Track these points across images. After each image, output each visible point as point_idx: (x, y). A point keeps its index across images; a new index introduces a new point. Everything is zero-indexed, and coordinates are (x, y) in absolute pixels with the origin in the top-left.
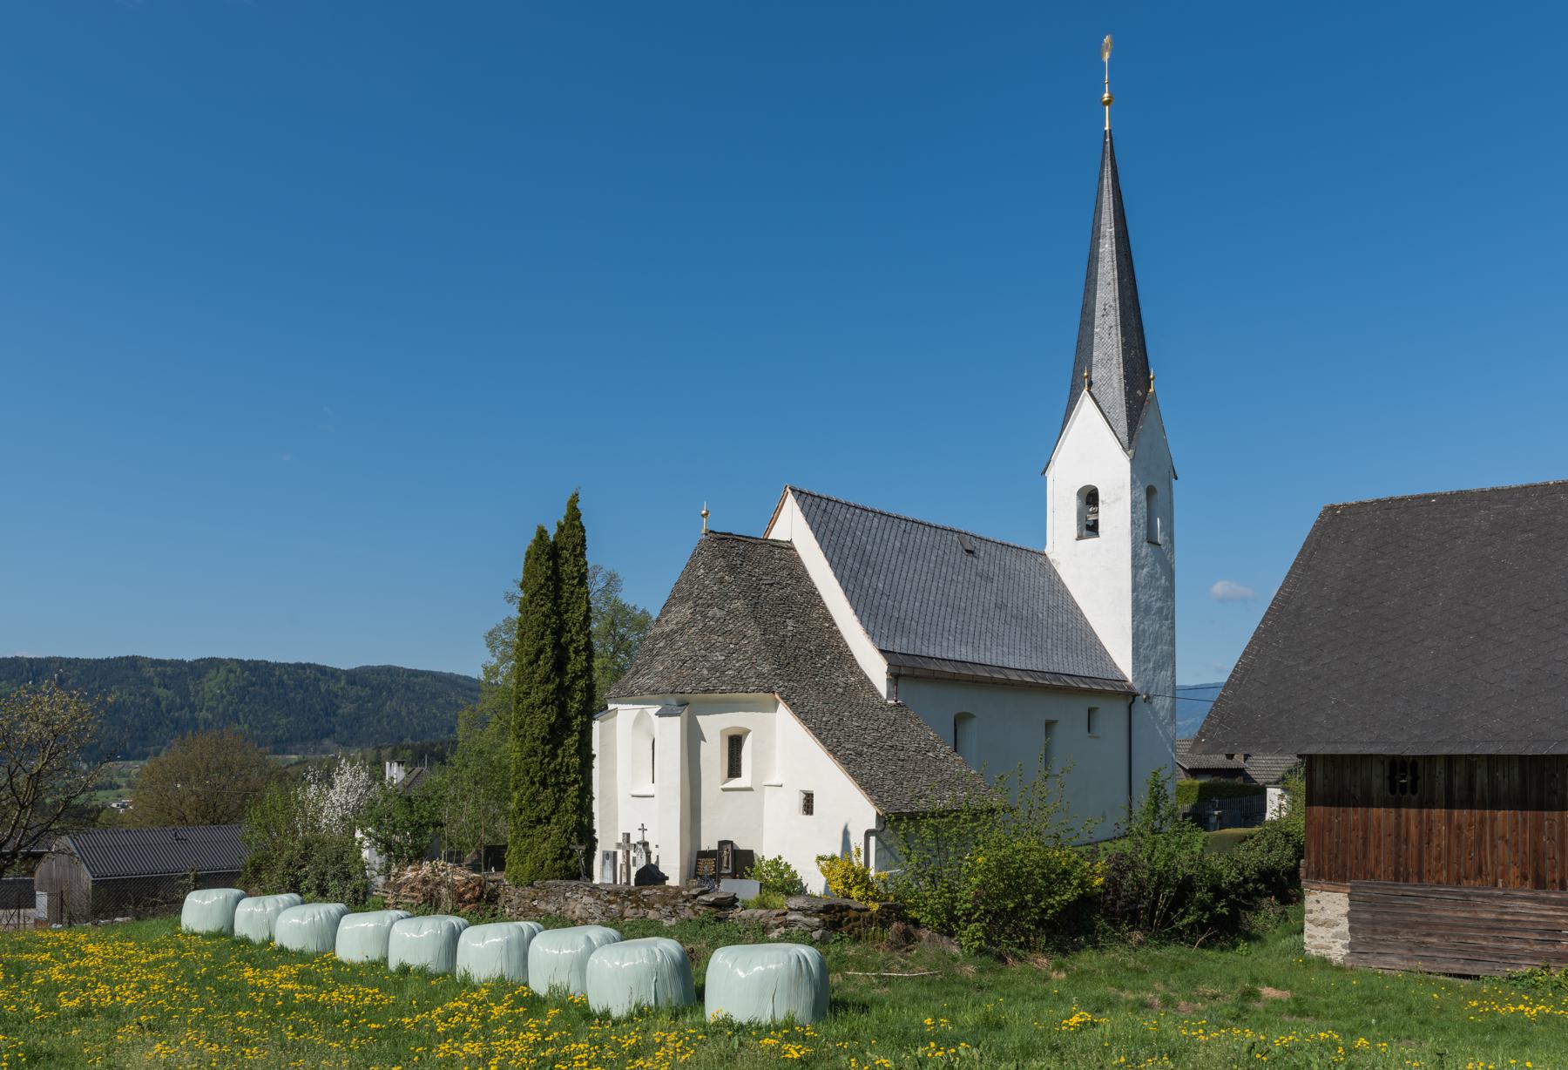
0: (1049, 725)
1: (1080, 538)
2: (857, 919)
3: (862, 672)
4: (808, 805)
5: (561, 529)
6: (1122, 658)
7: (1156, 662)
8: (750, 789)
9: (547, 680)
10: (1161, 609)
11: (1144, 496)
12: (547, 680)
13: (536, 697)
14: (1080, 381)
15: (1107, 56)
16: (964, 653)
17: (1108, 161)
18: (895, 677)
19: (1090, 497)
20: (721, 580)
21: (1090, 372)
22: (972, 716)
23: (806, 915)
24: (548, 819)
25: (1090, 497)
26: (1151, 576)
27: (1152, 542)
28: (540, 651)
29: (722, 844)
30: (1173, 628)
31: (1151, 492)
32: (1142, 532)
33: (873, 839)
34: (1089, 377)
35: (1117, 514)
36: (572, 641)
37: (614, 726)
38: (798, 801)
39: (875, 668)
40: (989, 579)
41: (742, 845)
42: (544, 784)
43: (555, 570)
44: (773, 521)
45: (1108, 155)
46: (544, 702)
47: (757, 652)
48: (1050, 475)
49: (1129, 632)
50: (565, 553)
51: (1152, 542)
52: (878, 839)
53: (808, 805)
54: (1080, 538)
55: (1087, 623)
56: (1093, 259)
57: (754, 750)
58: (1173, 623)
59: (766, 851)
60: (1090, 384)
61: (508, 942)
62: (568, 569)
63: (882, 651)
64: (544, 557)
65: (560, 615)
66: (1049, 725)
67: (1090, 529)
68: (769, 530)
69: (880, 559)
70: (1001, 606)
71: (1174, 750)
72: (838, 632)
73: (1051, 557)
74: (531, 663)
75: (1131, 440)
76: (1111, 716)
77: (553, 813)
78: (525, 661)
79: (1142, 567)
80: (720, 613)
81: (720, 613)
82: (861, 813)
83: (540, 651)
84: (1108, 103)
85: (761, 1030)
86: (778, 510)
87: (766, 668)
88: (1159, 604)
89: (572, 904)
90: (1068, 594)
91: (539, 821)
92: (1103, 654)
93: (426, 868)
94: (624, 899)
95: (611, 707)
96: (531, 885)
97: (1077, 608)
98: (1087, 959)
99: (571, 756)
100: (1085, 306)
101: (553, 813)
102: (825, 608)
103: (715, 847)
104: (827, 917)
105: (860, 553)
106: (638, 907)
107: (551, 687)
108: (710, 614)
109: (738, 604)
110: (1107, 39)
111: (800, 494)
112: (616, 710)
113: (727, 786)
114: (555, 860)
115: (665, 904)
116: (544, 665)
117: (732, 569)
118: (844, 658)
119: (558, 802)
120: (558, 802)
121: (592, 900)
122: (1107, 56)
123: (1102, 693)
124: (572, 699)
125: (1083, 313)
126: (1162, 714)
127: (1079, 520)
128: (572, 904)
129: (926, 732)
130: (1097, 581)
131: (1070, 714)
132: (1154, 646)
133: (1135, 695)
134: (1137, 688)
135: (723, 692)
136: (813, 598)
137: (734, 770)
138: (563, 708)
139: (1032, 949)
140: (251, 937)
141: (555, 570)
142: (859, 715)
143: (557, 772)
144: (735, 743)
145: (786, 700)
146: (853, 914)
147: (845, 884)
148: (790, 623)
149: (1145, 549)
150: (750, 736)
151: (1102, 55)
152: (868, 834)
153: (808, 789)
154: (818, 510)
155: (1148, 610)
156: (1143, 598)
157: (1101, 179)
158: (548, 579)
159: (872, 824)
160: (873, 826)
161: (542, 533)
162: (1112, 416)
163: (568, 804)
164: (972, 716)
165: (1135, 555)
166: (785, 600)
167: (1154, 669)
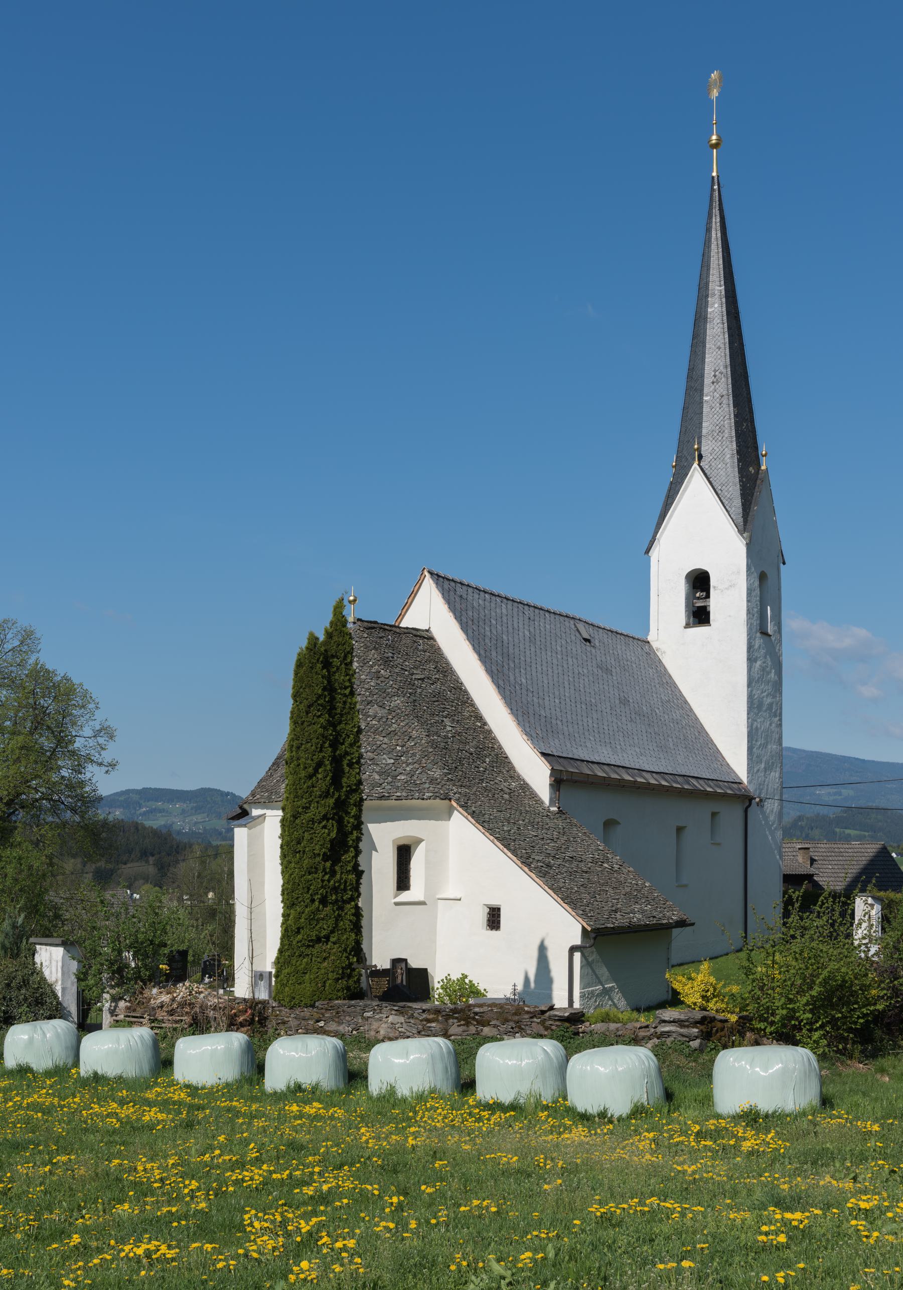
0: (680, 830)
1: (688, 626)
2: (722, 1029)
3: (519, 776)
4: (494, 919)
5: (329, 635)
6: (737, 761)
7: (767, 763)
8: (422, 903)
9: (326, 795)
10: (771, 705)
11: (757, 583)
12: (326, 795)
13: (317, 811)
14: (687, 455)
15: (715, 93)
16: (604, 755)
17: (716, 211)
18: (558, 782)
19: (699, 582)
20: (377, 676)
21: (700, 443)
22: (619, 823)
23: (682, 1026)
24: (327, 938)
25: (699, 582)
26: (763, 669)
27: (764, 633)
28: (320, 764)
29: (396, 962)
30: (780, 725)
31: (763, 577)
32: (756, 622)
33: (577, 956)
34: (699, 449)
35: (730, 600)
36: (347, 753)
37: (262, 832)
38: (482, 916)
39: (536, 774)
40: (608, 671)
41: (414, 964)
42: (324, 901)
43: (329, 678)
44: (406, 607)
45: (716, 204)
46: (325, 817)
47: (426, 755)
48: (654, 554)
49: (745, 731)
50: (336, 662)
51: (764, 633)
52: (583, 955)
53: (494, 919)
54: (688, 626)
55: (697, 719)
56: (700, 319)
57: (428, 862)
58: (780, 720)
59: (442, 970)
60: (700, 457)
61: (432, 1057)
62: (340, 677)
63: (544, 754)
64: (319, 666)
65: (334, 726)
66: (680, 830)
67: (700, 616)
68: (401, 616)
69: (517, 650)
70: (624, 702)
71: (781, 857)
72: (490, 732)
73: (655, 645)
74: (310, 777)
75: (745, 522)
76: (731, 817)
77: (332, 932)
78: (303, 774)
79: (755, 660)
80: (381, 713)
81: (381, 713)
82: (565, 929)
83: (320, 764)
84: (716, 146)
85: (804, 1114)
86: (413, 594)
87: (437, 773)
88: (769, 700)
89: (375, 1025)
90: (676, 687)
91: (318, 940)
92: (716, 755)
93: (182, 991)
94: (448, 1017)
95: (255, 812)
96: (313, 1006)
97: (686, 702)
98: (887, 1062)
99: (348, 872)
100: (691, 370)
101: (332, 932)
102: (473, 705)
103: (387, 966)
104: (702, 1027)
105: (499, 644)
106: (467, 1024)
107: (331, 801)
108: (371, 712)
109: (397, 701)
110: (714, 75)
111: (438, 578)
112: (263, 816)
113: (398, 899)
114: (337, 980)
115: (506, 1021)
116: (323, 780)
117: (386, 662)
118: (502, 761)
119: (338, 918)
120: (338, 918)
121: (402, 1019)
122: (715, 93)
123: (724, 796)
124: (348, 813)
125: (690, 377)
126: (772, 818)
127: (687, 606)
128: (375, 1025)
129: (589, 845)
130: (708, 675)
131: (696, 816)
132: (764, 746)
133: (751, 799)
134: (751, 789)
135: (399, 799)
136: (461, 697)
137: (403, 883)
138: (340, 822)
139: (851, 1057)
140: (34, 1066)
141: (329, 678)
142: (532, 824)
143: (335, 889)
144: (404, 853)
145: (465, 807)
146: (719, 1025)
147: (703, 997)
148: (447, 721)
149: (759, 641)
150: (423, 845)
151: (708, 92)
152: (573, 950)
153: (494, 902)
154: (454, 591)
155: (760, 706)
156: (757, 693)
157: (708, 230)
158: (324, 689)
159: (577, 939)
160: (578, 941)
161: (313, 639)
162: (725, 494)
163: (345, 924)
164: (619, 823)
165: (750, 647)
166: (437, 695)
167: (765, 769)
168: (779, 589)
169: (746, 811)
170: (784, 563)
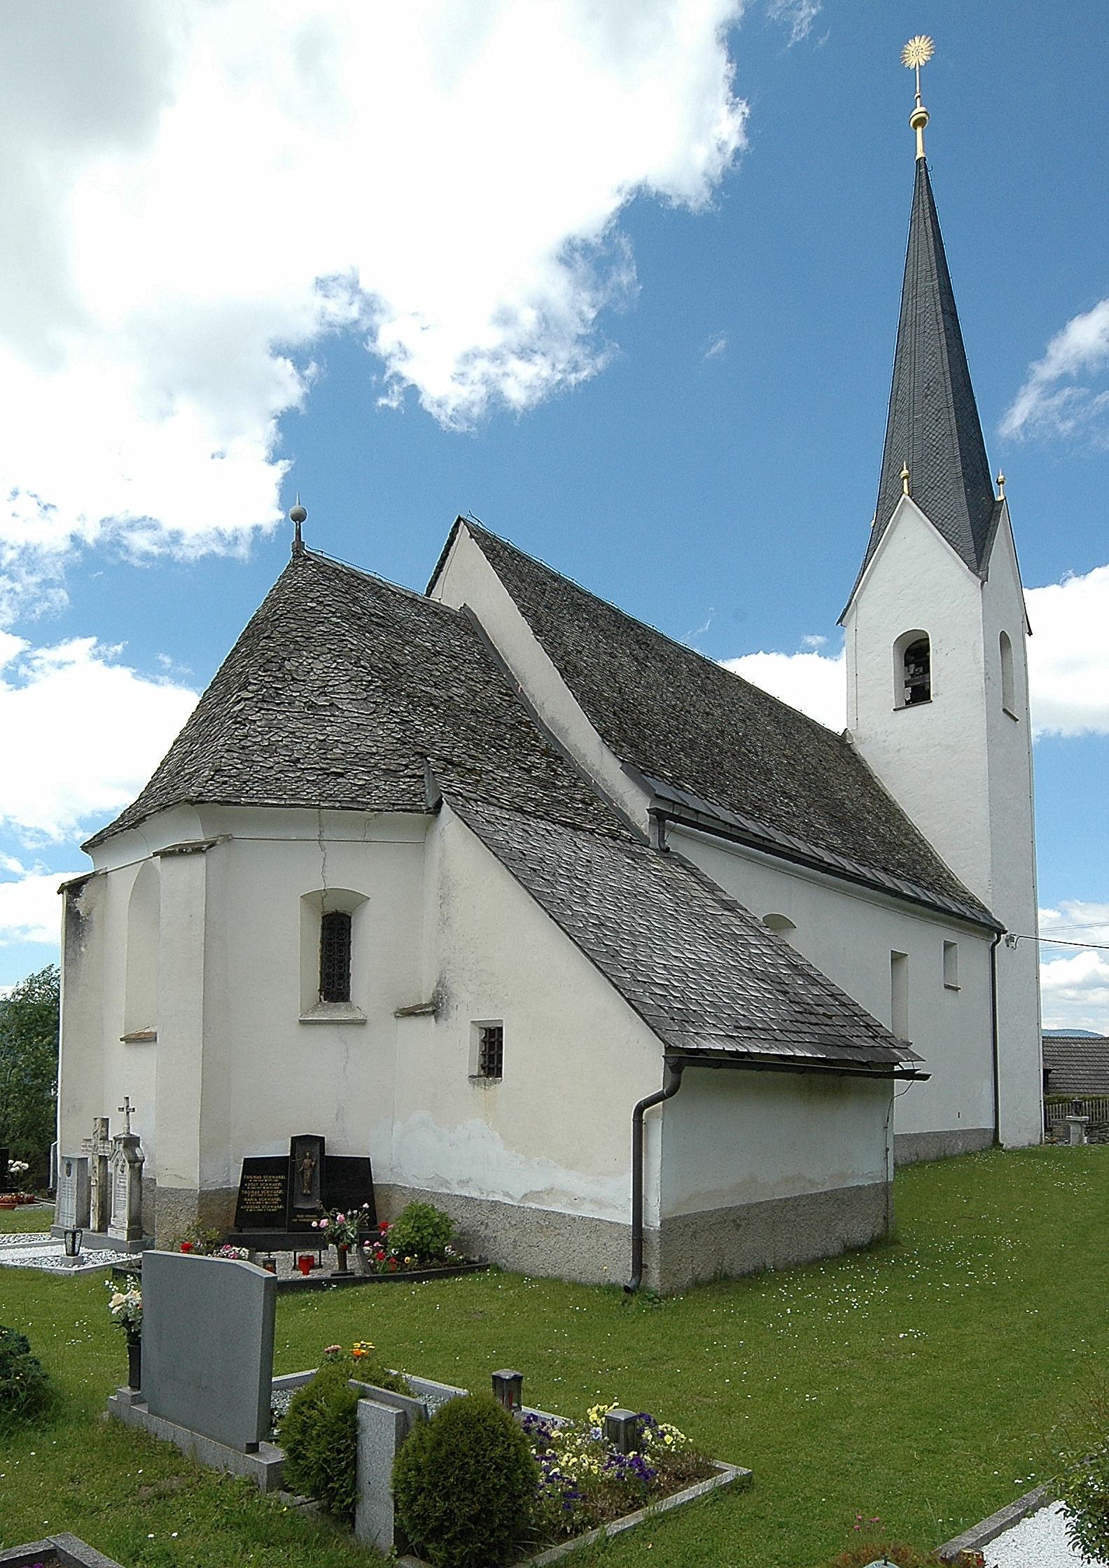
153: (488, 1015)
168: (1025, 653)
169: (993, 950)
170: (1030, 634)
